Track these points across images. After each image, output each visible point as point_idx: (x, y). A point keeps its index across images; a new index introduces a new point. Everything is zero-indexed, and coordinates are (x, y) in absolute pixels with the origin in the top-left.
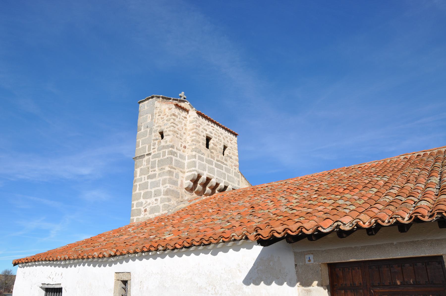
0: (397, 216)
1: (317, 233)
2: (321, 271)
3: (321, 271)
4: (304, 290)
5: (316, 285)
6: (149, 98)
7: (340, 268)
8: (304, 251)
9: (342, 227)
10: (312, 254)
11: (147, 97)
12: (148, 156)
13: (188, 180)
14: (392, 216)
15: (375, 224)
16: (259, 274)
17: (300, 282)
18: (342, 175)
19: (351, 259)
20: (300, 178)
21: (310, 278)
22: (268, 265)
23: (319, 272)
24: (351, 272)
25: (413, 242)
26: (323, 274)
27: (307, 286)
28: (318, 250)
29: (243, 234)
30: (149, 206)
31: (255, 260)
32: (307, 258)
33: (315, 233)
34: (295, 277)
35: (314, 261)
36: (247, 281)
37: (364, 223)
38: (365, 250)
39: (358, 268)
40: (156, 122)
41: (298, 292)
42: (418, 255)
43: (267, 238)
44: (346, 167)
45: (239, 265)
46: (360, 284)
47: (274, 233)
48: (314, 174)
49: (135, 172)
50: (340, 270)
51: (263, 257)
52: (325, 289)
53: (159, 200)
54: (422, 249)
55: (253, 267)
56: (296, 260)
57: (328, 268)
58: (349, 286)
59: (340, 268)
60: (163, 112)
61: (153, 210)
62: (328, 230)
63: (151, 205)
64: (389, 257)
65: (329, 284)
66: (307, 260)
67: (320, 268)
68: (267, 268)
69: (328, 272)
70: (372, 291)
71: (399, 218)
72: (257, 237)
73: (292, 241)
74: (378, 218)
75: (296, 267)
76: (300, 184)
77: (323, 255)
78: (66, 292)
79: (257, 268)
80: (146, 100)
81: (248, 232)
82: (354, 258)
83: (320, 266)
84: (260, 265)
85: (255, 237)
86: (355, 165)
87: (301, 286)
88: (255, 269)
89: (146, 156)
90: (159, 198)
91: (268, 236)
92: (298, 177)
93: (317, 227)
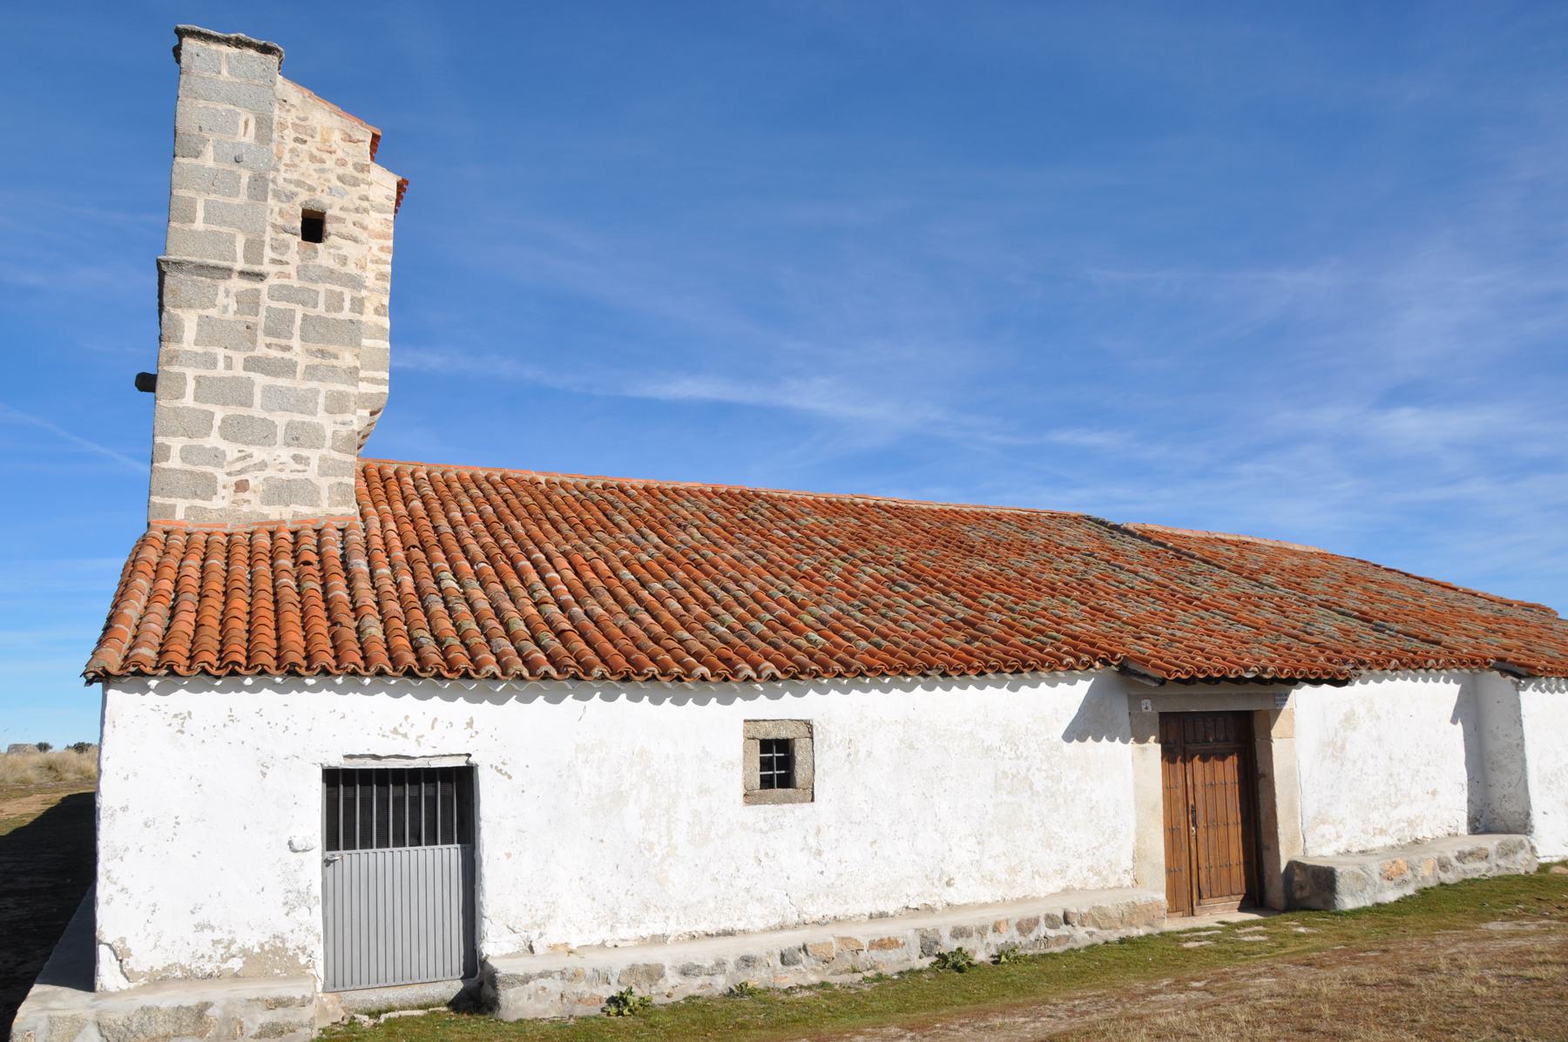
6: (249, 45)
11: (242, 35)
12: (248, 279)
13: (365, 408)
25: (1248, 694)
30: (262, 475)
36: (1069, 736)
40: (286, 158)
45: (1056, 709)
49: (170, 319)
53: (314, 462)
60: (318, 138)
61: (280, 492)
63: (269, 472)
66: (1143, 707)
78: (510, 777)
80: (227, 41)
89: (235, 277)
90: (314, 455)
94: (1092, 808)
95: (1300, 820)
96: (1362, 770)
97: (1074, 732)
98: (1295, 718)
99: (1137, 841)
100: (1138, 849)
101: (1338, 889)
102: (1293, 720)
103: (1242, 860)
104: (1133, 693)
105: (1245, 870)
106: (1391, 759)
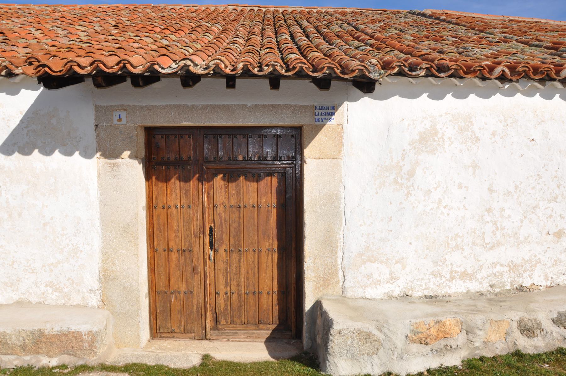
0: (275, 63)
1: (150, 73)
2: (137, 136)
3: (137, 136)
4: (108, 165)
5: (127, 157)
7: (162, 135)
8: (112, 106)
9: (192, 69)
10: (125, 110)
14: (269, 62)
15: (241, 71)
16: (30, 137)
17: (102, 151)
18: (148, 13)
19: (185, 121)
20: (79, 8)
21: (118, 146)
22: (48, 123)
23: (133, 137)
24: (178, 141)
25: (272, 106)
26: (139, 141)
27: (113, 158)
28: (135, 105)
29: (2, 67)
31: (24, 114)
32: (116, 116)
33: (145, 74)
34: (95, 145)
35: (127, 122)
37: (226, 67)
38: (207, 111)
39: (188, 136)
41: (98, 166)
42: (275, 123)
43: (58, 74)
44: (152, 5)
46: (190, 158)
47: (74, 65)
48: (102, 5)
50: (162, 137)
51: (40, 110)
52: (140, 164)
54: (281, 116)
55: (19, 125)
56: (98, 118)
57: (145, 134)
58: (174, 160)
59: (162, 135)
62: (169, 71)
64: (239, 123)
65: (144, 156)
67: (136, 132)
68: (45, 127)
69: (144, 140)
70: (204, 167)
71: (278, 66)
72: (40, 70)
73: (103, 84)
74: (249, 62)
75: (96, 129)
76: (81, 14)
77: (142, 112)
79: (26, 128)
81: (12, 64)
82: (190, 121)
83: (136, 130)
84: (33, 123)
85: (36, 69)
86: (166, 5)
87: (103, 158)
88: (24, 128)
91: (60, 71)
92: (76, 6)
93: (151, 64)
94: (45, 225)
95: (340, 254)
96: (440, 201)
97: (14, 144)
98: (345, 136)
99: (104, 261)
100: (105, 270)
101: (331, 350)
102: (342, 138)
103: (276, 289)
104: (103, 103)
105: (279, 299)
106: (491, 190)
